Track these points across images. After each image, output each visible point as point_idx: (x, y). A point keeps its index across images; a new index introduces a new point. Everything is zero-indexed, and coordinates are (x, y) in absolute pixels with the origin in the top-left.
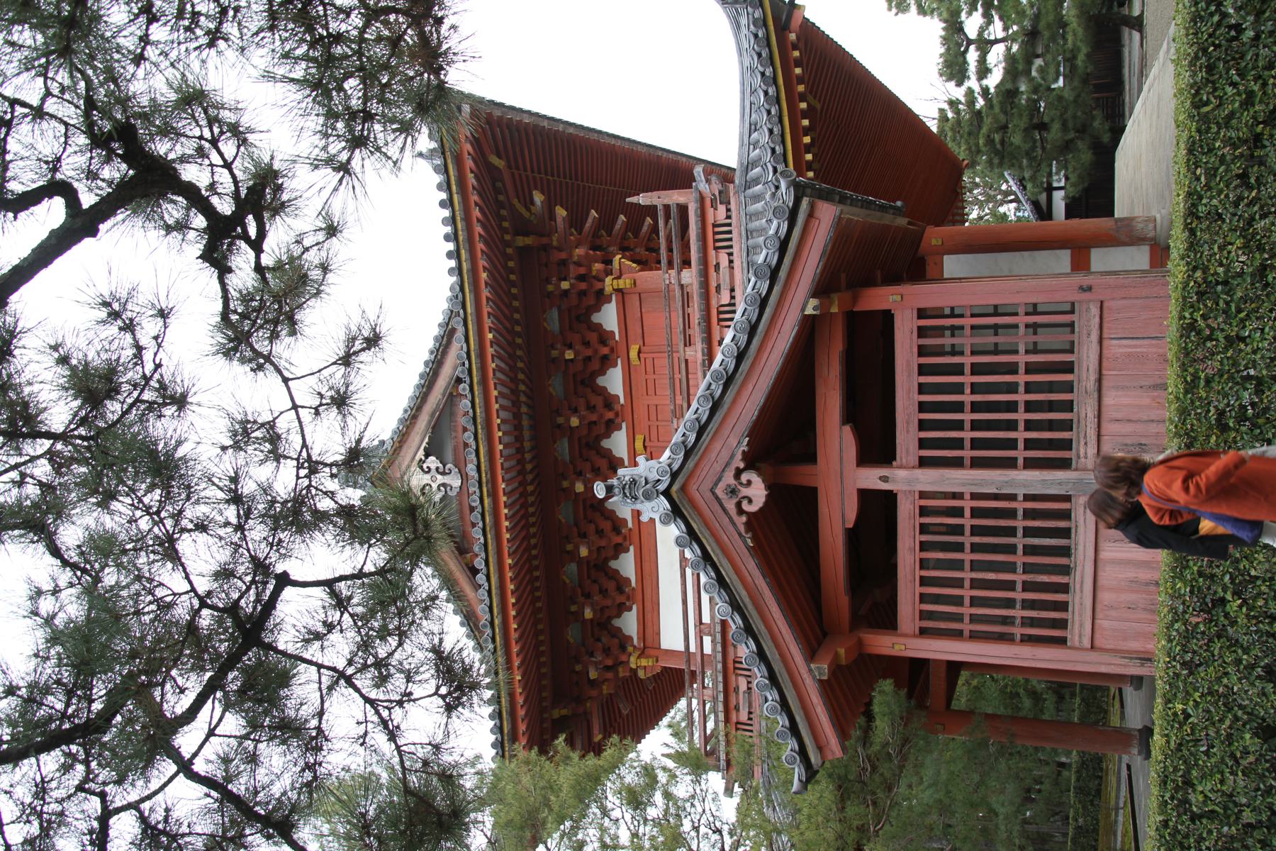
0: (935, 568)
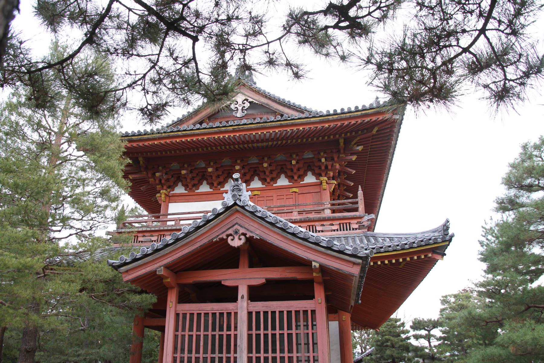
0: (205, 319)
